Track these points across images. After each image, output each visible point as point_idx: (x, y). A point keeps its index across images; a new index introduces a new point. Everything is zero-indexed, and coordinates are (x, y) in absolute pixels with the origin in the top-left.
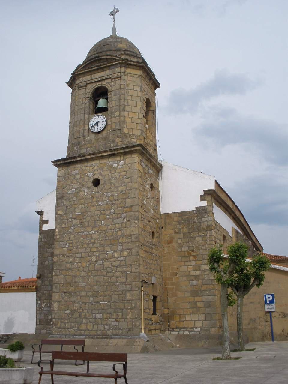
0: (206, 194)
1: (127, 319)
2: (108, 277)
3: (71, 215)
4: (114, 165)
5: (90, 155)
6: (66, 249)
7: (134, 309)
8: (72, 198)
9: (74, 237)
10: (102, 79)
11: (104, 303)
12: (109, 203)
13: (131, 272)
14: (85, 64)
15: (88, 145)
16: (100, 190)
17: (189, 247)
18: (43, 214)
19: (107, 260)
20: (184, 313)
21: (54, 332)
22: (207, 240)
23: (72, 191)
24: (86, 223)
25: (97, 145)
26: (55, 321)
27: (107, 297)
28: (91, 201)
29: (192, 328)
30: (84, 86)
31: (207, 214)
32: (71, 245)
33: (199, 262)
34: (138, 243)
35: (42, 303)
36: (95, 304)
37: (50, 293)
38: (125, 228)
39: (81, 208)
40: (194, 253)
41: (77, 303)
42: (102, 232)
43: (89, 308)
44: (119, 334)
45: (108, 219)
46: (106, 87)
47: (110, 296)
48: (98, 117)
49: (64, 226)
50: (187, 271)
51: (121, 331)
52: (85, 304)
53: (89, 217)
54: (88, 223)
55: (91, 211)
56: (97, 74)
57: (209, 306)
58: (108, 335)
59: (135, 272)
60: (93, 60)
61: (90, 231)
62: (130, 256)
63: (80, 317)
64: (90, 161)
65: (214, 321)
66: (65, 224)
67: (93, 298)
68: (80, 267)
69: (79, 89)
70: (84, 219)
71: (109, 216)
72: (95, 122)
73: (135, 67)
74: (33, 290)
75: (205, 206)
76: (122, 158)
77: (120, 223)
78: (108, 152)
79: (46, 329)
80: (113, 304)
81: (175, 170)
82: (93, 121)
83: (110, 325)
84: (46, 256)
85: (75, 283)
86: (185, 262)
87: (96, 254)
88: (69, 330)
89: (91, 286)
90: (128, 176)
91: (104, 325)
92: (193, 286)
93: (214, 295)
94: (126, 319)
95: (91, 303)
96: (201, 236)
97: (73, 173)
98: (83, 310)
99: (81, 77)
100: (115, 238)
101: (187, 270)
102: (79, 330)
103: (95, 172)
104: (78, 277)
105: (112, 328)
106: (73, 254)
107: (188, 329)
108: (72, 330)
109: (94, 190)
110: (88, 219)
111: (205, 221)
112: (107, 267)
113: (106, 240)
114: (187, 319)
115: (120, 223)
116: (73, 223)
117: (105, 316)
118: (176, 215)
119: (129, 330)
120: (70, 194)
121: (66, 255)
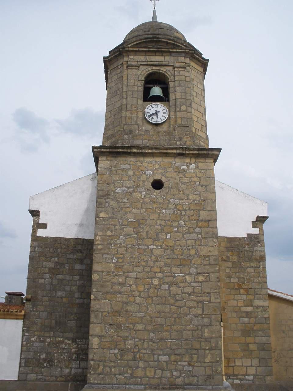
0: (259, 221)
1: (205, 362)
2: (177, 306)
3: (120, 220)
4: (182, 167)
5: (151, 148)
6: (113, 265)
7: (214, 350)
8: (122, 199)
10: (160, 63)
11: (171, 340)
12: (177, 213)
14: (140, 42)
15: (145, 137)
16: (164, 195)
17: (239, 278)
18: (39, 215)
19: (174, 284)
20: (233, 356)
21: (91, 379)
22: (259, 273)
23: (122, 190)
24: (144, 234)
25: (157, 139)
26: (94, 364)
27: (175, 333)
30: (136, 66)
31: (260, 243)
32: (120, 260)
33: (251, 297)
34: (218, 266)
35: (31, 336)
36: (158, 342)
37: (45, 322)
38: (200, 247)
39: (136, 213)
40: (245, 285)
41: (130, 340)
42: (167, 247)
43: (148, 346)
44: (194, 383)
45: (176, 232)
46: (166, 74)
47: (181, 331)
48: (157, 107)
49: (109, 233)
50: (237, 306)
51: (196, 378)
52: (143, 341)
53: (148, 226)
55: (151, 219)
56: (153, 57)
57: (264, 350)
58: (178, 385)
59: (215, 303)
60: (150, 40)
61: (150, 245)
62: (207, 281)
63: (134, 359)
64: (149, 156)
65: (270, 367)
66: (112, 232)
67: (155, 334)
68: (135, 291)
69: (129, 68)
70: (141, 228)
71: (177, 229)
72: (153, 111)
73: (198, 63)
74: (18, 317)
75: (257, 234)
76: (193, 160)
77: (193, 240)
78: (176, 150)
79: (36, 373)
80: (184, 343)
81: (222, 188)
82: (151, 110)
83: (180, 371)
84: (41, 271)
85: (128, 311)
86: (234, 295)
87: (160, 275)
88: (116, 377)
89: (152, 317)
90: (202, 184)
91: (172, 370)
92: (244, 325)
93: (268, 337)
94: (203, 362)
95: (152, 340)
96: (252, 267)
97: (124, 166)
98: (139, 350)
99: (131, 55)
100: (186, 257)
101: (237, 304)
102: (134, 378)
103: (156, 172)
104: (132, 304)
105: (183, 375)
106: (124, 273)
107: (239, 377)
108: (121, 376)
109: (155, 194)
110: (147, 228)
111: (258, 251)
112: (175, 293)
113: (173, 258)
114: (237, 364)
115: (193, 240)
116: (123, 232)
117: (173, 358)
118: (224, 240)
119: (207, 378)
120: (118, 193)
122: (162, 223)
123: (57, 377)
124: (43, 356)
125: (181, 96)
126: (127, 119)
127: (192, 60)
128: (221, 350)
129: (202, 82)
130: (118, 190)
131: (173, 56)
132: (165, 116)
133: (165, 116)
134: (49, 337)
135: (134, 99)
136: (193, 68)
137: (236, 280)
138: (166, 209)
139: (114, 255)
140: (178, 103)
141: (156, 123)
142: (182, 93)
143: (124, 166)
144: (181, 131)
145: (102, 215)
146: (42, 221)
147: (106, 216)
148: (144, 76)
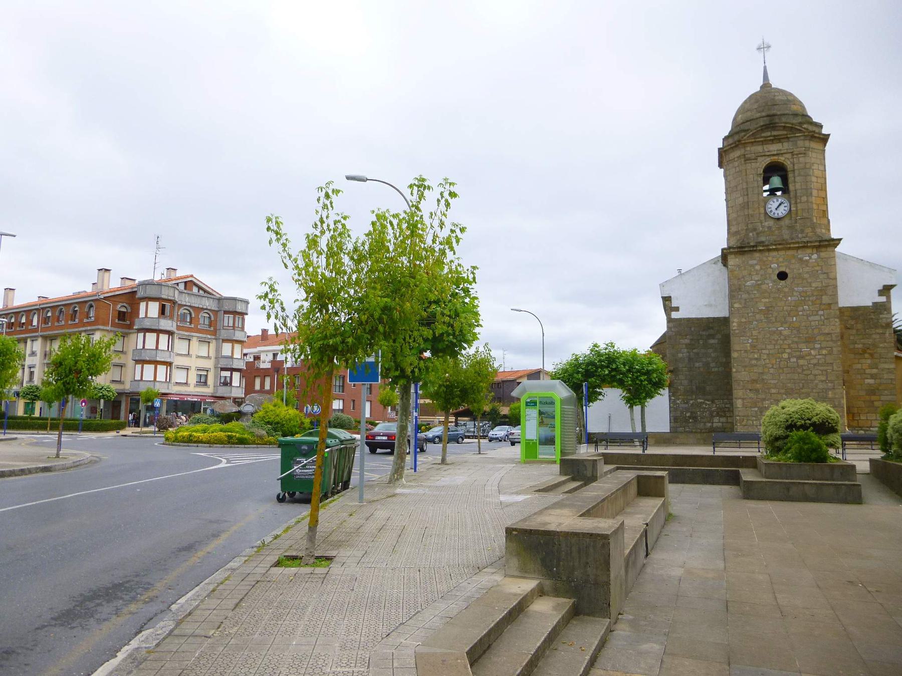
8: (752, 291)
9: (759, 332)
10: (779, 152)
13: (833, 371)
24: (773, 319)
28: (777, 296)
29: (867, 427)
32: (755, 341)
49: (744, 320)
54: (776, 319)
66: (746, 319)
69: (747, 162)
87: (788, 351)
96: (878, 333)
97: (751, 262)
103: (780, 265)
110: (775, 314)
121: (749, 351)
122: (789, 308)
123: (701, 430)
124: (688, 414)
128: (843, 407)
129: (823, 161)
130: (748, 283)
134: (692, 400)
137: (860, 346)
138: (791, 296)
139: (749, 337)
140: (798, 195)
143: (751, 262)
145: (736, 305)
146: (674, 304)
147: (740, 306)
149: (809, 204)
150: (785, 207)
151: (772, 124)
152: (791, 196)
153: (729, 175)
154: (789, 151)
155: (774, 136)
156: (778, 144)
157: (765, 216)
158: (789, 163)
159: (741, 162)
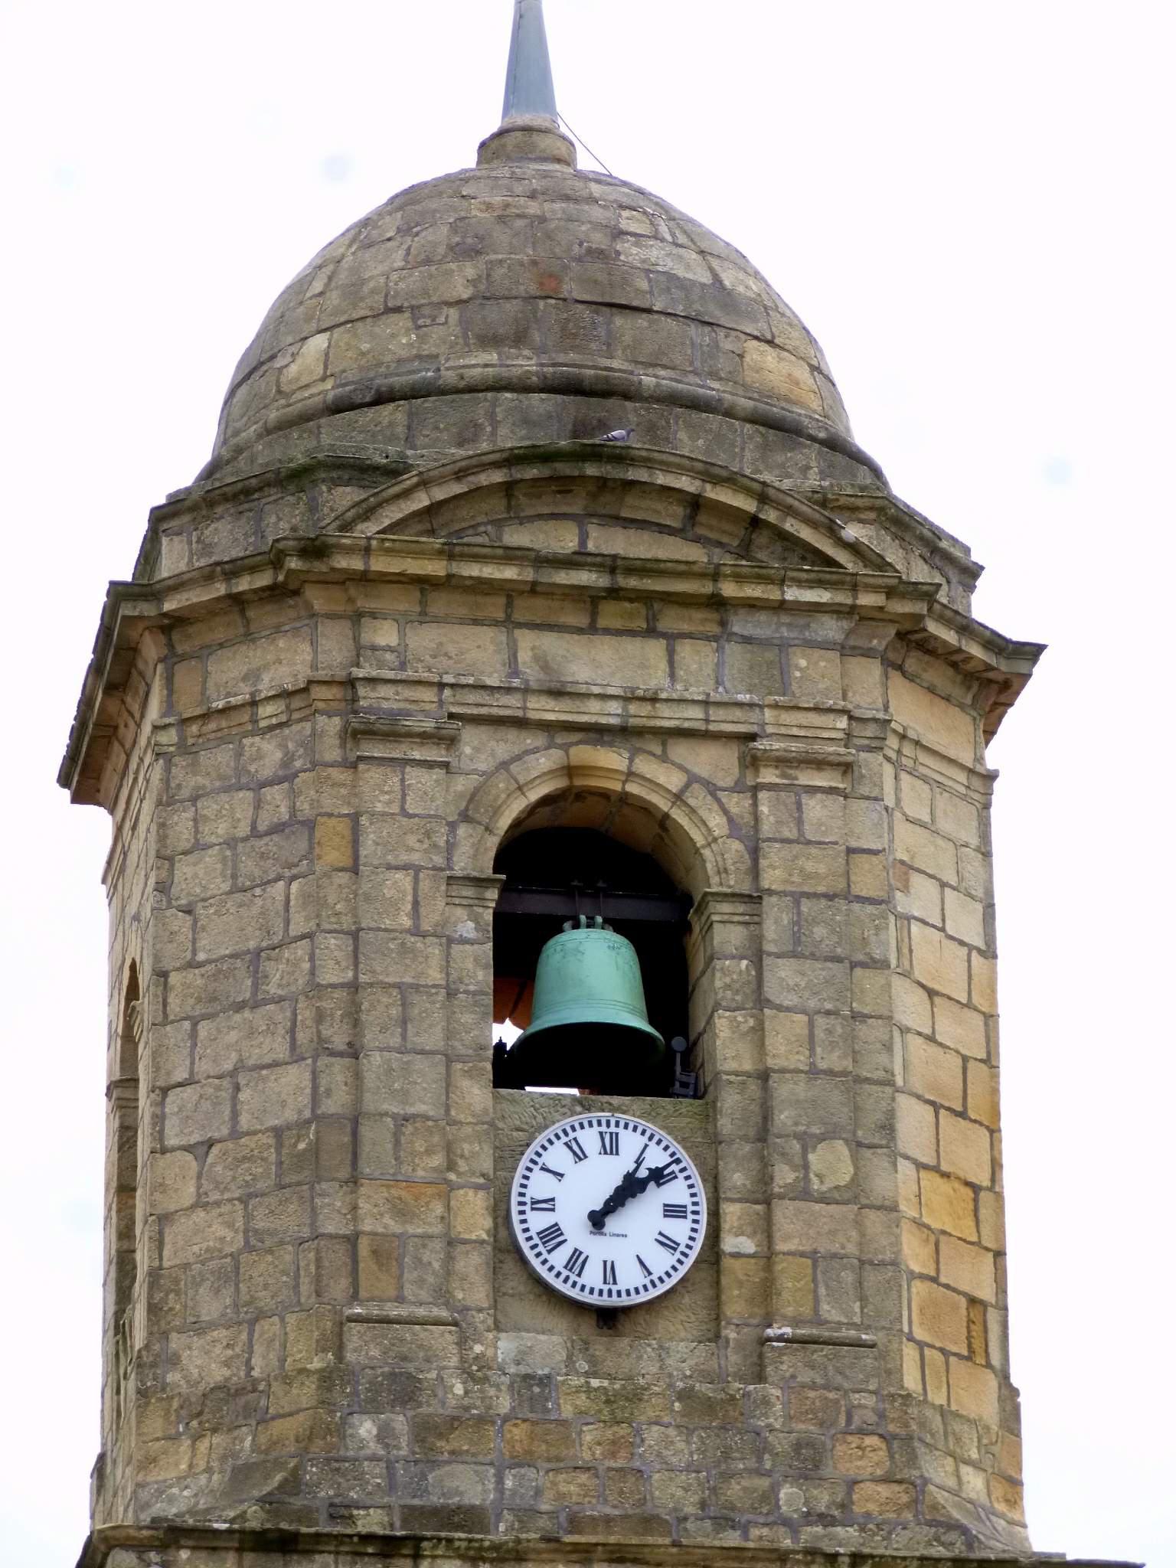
10: (639, 713)
82: (559, 1175)
125: (812, 1050)
126: (366, 1263)
127: (900, 668)
131: (747, 640)
132: (683, 1240)
133: (683, 1240)
135: (420, 1063)
136: (908, 750)
140: (783, 1118)
141: (605, 1301)
142: (821, 1021)
144: (813, 1386)
148: (502, 833)
149: (873, 1219)
150: (672, 1211)
151: (595, 454)
152: (725, 1125)
153: (199, 847)
154: (727, 722)
155: (612, 564)
156: (633, 647)
157: (495, 1270)
158: (717, 822)
159: (310, 744)
